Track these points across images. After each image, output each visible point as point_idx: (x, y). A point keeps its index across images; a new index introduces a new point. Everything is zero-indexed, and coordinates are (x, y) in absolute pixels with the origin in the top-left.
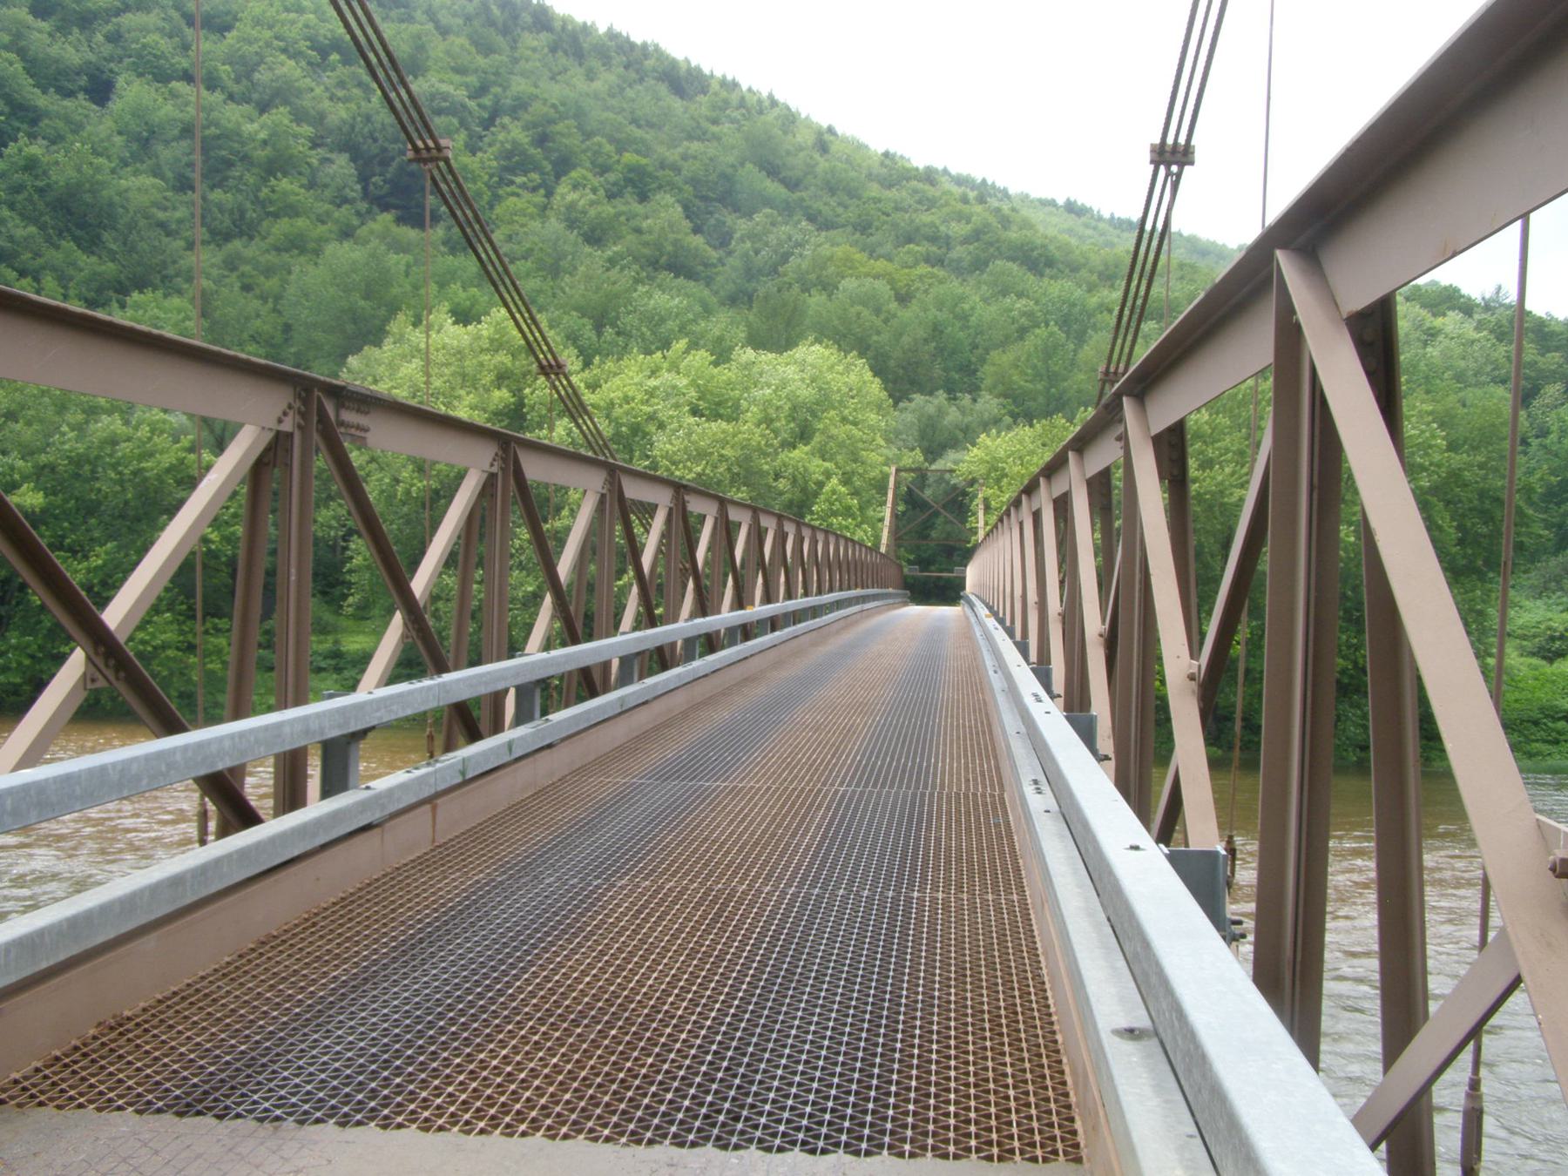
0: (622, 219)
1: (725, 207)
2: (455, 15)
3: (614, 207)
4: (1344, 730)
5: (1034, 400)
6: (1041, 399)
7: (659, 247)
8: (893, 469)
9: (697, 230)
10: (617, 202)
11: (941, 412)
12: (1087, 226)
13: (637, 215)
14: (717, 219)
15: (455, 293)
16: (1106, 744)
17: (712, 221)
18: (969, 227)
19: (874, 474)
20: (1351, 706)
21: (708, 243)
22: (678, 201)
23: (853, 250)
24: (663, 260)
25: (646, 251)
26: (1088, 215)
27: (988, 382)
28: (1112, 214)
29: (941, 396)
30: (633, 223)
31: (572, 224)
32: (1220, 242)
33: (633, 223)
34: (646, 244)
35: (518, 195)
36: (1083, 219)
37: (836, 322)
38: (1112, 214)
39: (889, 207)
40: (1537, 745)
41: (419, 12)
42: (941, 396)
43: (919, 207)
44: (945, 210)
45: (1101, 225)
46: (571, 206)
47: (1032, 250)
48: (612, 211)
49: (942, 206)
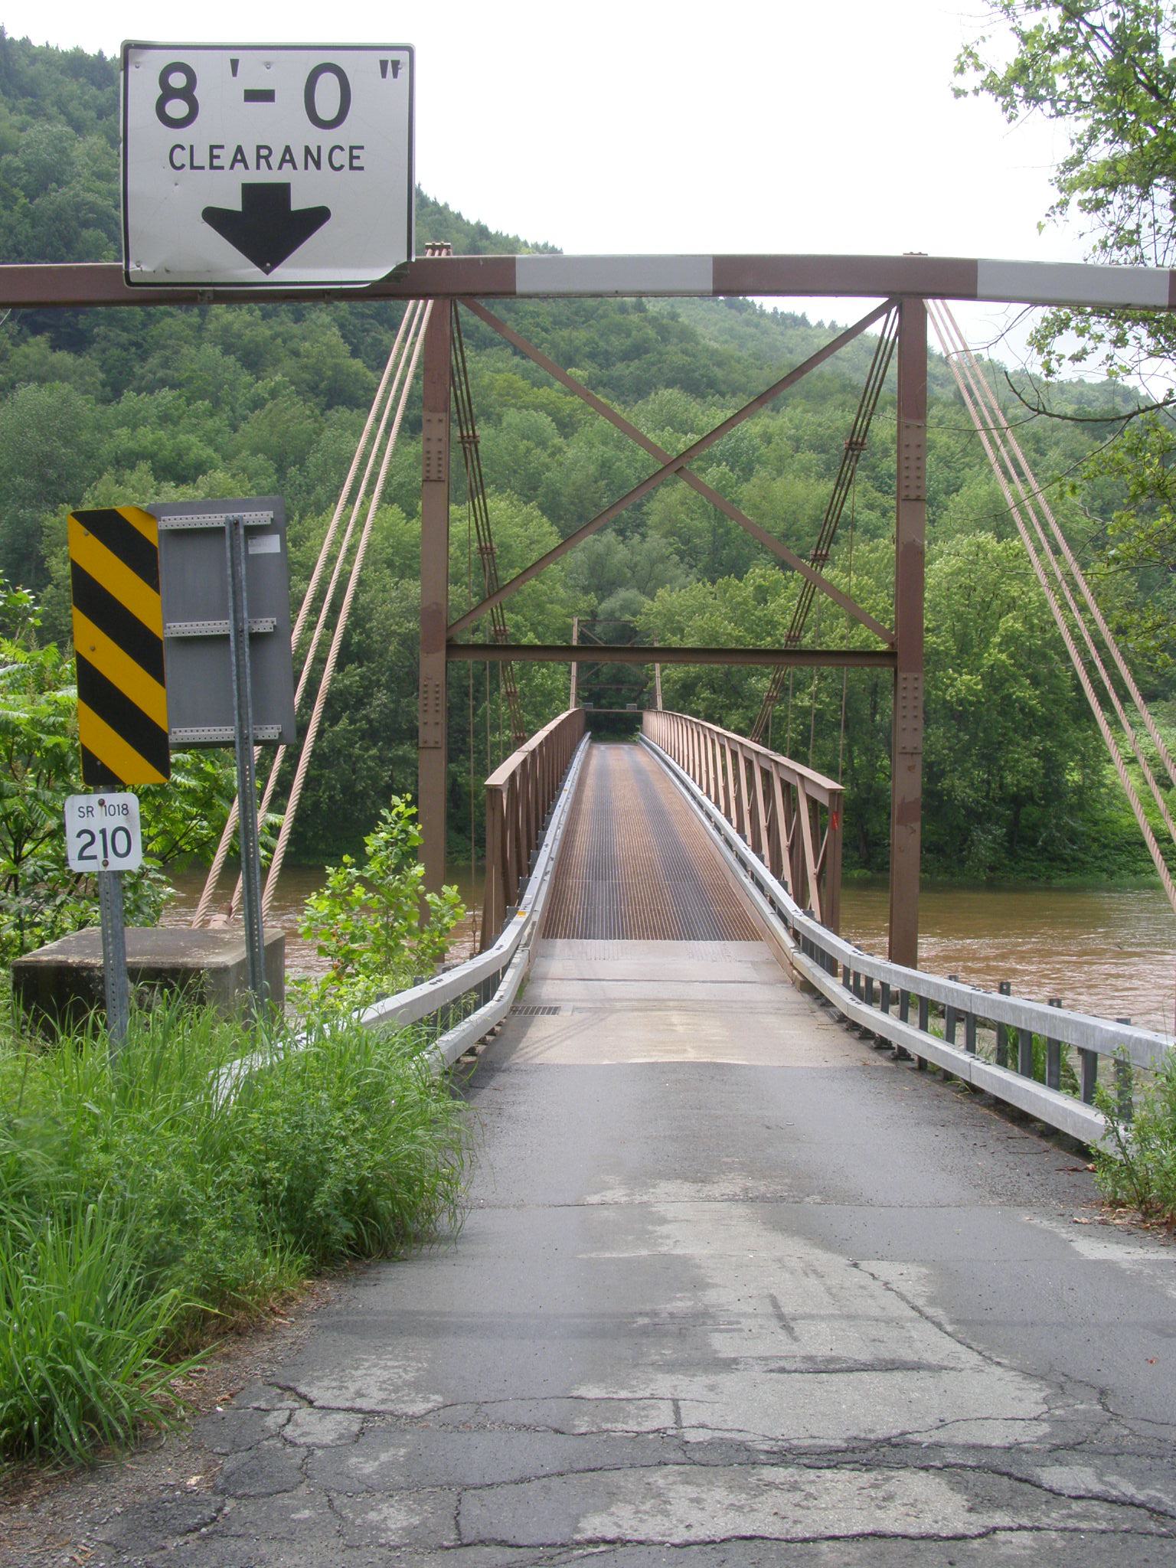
0: (279, 341)
1: (381, 324)
2: (86, 106)
3: (270, 328)
4: (977, 854)
5: (700, 537)
6: (709, 537)
7: (318, 372)
8: (576, 620)
9: (355, 353)
10: (273, 321)
11: (609, 551)
12: (748, 323)
13: (295, 336)
14: (373, 337)
15: (144, 435)
16: (768, 863)
17: (369, 340)
18: (629, 342)
19: (559, 624)
20: (984, 832)
21: (368, 367)
22: (334, 319)
23: (517, 377)
24: (323, 385)
25: (306, 376)
26: (750, 311)
27: (653, 520)
28: (775, 308)
29: (610, 536)
30: (291, 345)
31: (228, 350)
32: (916, 252)
33: (291, 345)
34: (305, 368)
35: (171, 315)
36: (745, 315)
37: (507, 458)
38: (775, 308)
39: (547, 321)
40: (1142, 864)
41: (48, 101)
42: (610, 536)
43: (577, 318)
44: (604, 322)
45: (764, 322)
46: (226, 329)
47: (694, 371)
48: (268, 333)
49: (602, 317)
